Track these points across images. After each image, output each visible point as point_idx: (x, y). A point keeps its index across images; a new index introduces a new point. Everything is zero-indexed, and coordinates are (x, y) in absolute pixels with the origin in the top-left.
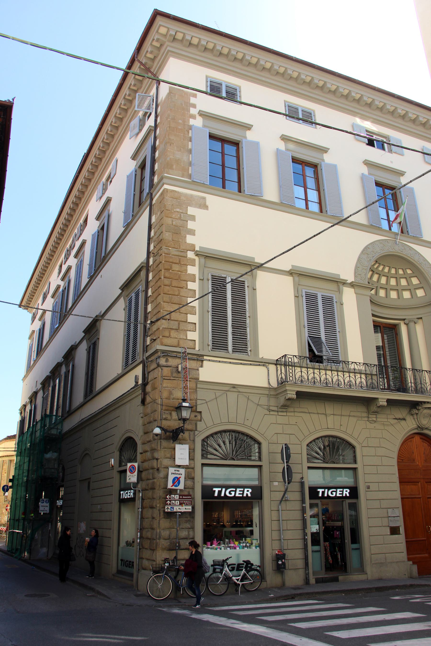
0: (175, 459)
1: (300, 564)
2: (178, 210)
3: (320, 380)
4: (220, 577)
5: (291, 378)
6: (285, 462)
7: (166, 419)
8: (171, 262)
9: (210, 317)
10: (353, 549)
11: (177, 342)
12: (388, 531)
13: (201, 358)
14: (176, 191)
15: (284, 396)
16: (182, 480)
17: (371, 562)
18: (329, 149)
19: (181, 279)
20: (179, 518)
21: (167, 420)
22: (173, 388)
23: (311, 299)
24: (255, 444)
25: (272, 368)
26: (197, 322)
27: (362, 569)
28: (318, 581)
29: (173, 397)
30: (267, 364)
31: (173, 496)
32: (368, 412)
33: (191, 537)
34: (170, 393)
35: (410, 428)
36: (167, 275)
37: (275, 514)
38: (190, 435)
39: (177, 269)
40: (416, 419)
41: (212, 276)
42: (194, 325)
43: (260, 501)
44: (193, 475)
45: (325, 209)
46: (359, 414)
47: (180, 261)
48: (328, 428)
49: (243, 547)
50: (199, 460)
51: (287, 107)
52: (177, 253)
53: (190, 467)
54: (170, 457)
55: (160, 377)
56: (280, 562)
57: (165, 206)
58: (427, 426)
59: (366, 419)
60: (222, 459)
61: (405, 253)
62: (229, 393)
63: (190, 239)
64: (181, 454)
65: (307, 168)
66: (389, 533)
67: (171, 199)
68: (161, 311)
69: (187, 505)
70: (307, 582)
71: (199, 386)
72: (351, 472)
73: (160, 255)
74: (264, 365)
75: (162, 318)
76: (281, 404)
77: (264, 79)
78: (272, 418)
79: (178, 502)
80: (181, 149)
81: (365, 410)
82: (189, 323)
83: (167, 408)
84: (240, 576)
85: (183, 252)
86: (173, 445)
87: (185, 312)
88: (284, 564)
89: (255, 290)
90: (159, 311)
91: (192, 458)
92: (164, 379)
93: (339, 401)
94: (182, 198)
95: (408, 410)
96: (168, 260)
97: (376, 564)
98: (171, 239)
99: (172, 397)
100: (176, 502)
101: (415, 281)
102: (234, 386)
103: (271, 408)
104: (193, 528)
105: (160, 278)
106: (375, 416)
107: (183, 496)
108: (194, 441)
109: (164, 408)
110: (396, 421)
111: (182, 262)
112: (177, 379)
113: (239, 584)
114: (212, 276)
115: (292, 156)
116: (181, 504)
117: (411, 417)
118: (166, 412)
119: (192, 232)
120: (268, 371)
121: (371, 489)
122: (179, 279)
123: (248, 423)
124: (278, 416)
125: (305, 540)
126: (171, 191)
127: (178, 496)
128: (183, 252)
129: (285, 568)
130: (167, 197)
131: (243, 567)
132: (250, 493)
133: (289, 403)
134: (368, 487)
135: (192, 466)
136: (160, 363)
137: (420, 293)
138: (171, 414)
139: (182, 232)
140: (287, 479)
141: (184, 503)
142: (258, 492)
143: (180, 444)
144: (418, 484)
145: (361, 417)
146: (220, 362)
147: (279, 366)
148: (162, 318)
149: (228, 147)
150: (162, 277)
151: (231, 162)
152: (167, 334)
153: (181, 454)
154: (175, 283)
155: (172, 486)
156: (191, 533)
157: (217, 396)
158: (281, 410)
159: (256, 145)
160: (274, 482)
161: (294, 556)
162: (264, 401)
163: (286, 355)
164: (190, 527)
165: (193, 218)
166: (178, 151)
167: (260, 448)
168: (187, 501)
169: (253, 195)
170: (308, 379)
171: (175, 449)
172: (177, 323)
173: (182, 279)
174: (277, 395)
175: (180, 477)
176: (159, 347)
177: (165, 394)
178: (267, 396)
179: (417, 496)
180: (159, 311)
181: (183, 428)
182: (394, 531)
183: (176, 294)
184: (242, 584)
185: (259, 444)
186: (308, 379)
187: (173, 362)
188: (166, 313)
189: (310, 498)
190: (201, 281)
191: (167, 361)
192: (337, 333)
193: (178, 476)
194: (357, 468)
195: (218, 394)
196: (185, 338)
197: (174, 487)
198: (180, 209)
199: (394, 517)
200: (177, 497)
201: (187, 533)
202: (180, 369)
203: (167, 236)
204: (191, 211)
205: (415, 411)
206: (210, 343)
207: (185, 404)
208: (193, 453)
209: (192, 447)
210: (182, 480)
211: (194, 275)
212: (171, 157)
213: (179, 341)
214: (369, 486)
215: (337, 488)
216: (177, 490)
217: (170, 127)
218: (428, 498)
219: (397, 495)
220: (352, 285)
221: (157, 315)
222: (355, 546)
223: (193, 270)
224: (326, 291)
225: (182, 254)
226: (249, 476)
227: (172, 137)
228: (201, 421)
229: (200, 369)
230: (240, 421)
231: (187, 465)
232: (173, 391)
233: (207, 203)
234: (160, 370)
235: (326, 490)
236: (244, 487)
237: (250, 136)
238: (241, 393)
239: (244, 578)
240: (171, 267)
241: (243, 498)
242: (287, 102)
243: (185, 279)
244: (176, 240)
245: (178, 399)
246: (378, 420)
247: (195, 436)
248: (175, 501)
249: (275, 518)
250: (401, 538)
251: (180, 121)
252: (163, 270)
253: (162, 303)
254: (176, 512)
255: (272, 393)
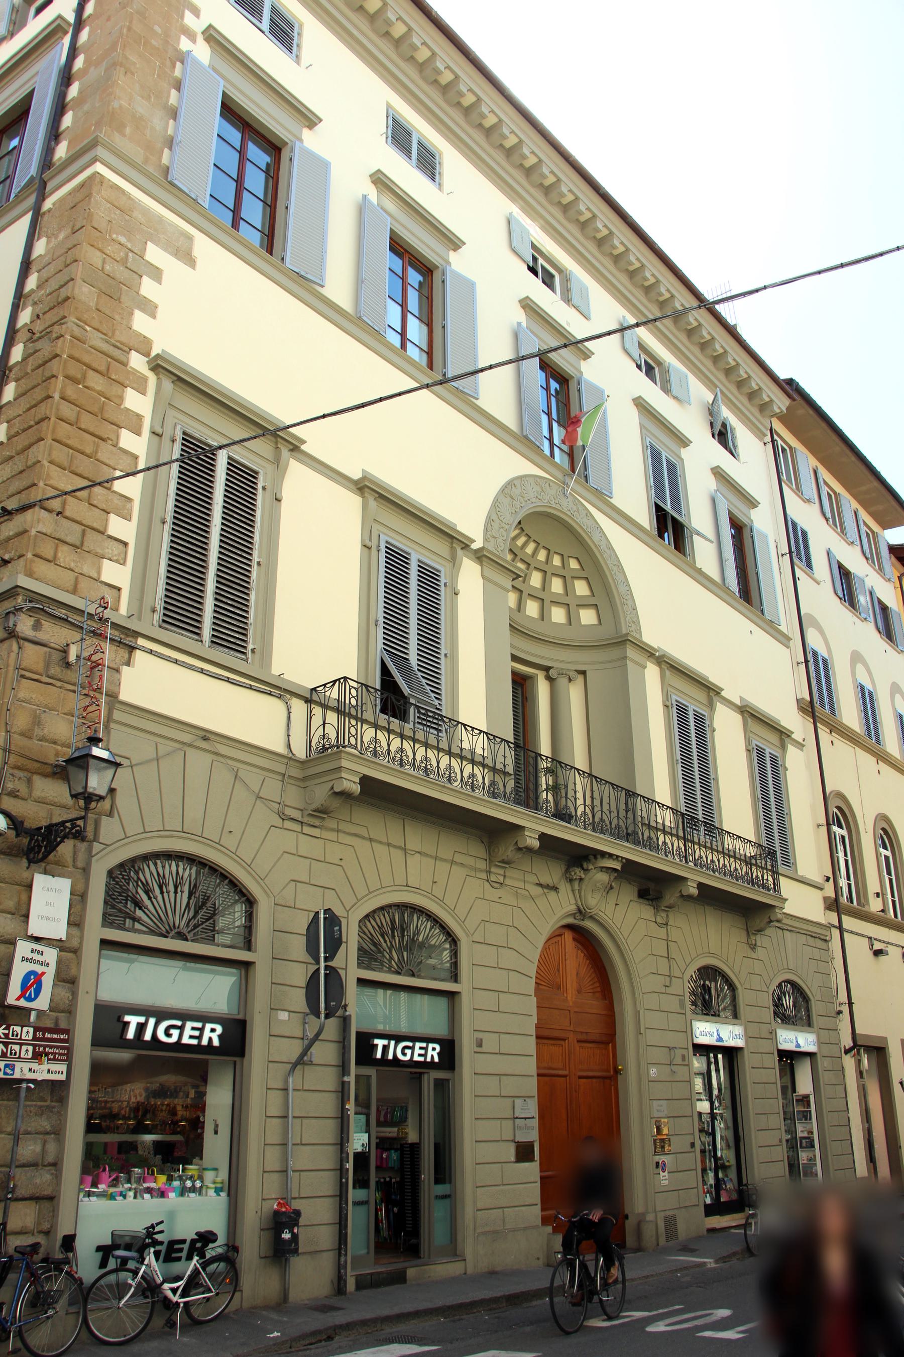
0: (27, 916)
1: (325, 1237)
2: (123, 240)
3: (414, 758)
4: (131, 1286)
5: (353, 741)
6: (322, 959)
7: (13, 794)
8: (85, 364)
9: (167, 538)
10: (437, 1197)
11: (72, 582)
12: (510, 1152)
13: (128, 640)
14: (123, 191)
15: (331, 784)
16: (48, 982)
17: (475, 1229)
18: (465, 244)
19: (106, 416)
20: (27, 1098)
21: (16, 797)
22: (46, 706)
23: (396, 561)
24: (236, 902)
25: (299, 707)
26: (131, 541)
27: (453, 1251)
28: (361, 1285)
29: (41, 733)
30: (288, 696)
31: (18, 1029)
32: (490, 860)
33: (50, 1158)
34: (37, 721)
35: (565, 911)
36: (70, 392)
37: (275, 1098)
38: (75, 853)
39: (98, 388)
40: (577, 892)
41: (184, 433)
42: (121, 546)
43: (237, 1059)
44: (73, 971)
45: (440, 372)
46: (470, 861)
47: (108, 369)
48: (407, 886)
49: (183, 1192)
50: (95, 929)
51: (390, 119)
52: (105, 347)
53: (67, 945)
54: (13, 910)
55: (11, 668)
56: (286, 1236)
57: (90, 217)
58: (594, 911)
59: (484, 876)
60: (152, 932)
61: (579, 522)
62: (190, 752)
63: (140, 322)
64: (48, 904)
65: (417, 268)
66: (513, 1159)
67: (108, 205)
68: (41, 484)
69: (54, 1059)
70: (340, 1288)
71: (117, 715)
72: (442, 1003)
73: (58, 338)
74: (280, 697)
75: (41, 503)
76: (314, 806)
77: (355, 32)
78: (288, 838)
79: (30, 1048)
80: (150, 97)
81: (482, 853)
82: (110, 537)
83: (21, 761)
84: (181, 1279)
85: (118, 348)
86: (26, 874)
87: (104, 506)
88: (295, 1237)
89: (278, 500)
90: (35, 485)
91: (75, 922)
92: (23, 676)
93: (433, 823)
94: (136, 214)
95: (564, 868)
96: (77, 355)
97: (484, 1233)
98: (92, 304)
99: (38, 732)
100: (24, 1048)
101: (581, 588)
102: (206, 735)
103: (289, 812)
104: (58, 1133)
105: (49, 397)
106: (501, 871)
107: (45, 1030)
108: (86, 871)
109: (13, 759)
110: (540, 889)
111: (116, 375)
112: (59, 684)
113: (178, 1304)
114: (184, 433)
115: (392, 231)
116: (37, 1056)
117: (568, 885)
118: (17, 772)
119: (150, 309)
120: (290, 712)
121: (484, 1048)
122: (99, 414)
123: (230, 842)
124: (300, 836)
125: (342, 1171)
126: (111, 187)
127: (31, 1030)
128: (118, 348)
129: (296, 1251)
130: (99, 198)
131: (181, 1250)
132: (219, 1036)
133: (336, 803)
134: (480, 1044)
135: (75, 943)
136: (18, 629)
137: (588, 617)
138: (29, 781)
139: (124, 298)
140: (322, 1005)
141: (47, 1054)
142: (236, 1036)
143: (46, 872)
144: (563, 1043)
145: (475, 870)
146: (176, 662)
147: (317, 711)
148: (41, 503)
149: (261, 144)
150: (57, 396)
151: (255, 181)
152: (47, 550)
153: (48, 904)
154: (87, 421)
155: (18, 999)
156: (52, 1147)
157: (160, 754)
158: (307, 819)
159: (322, 167)
160: (280, 1012)
161: (317, 1216)
162: (273, 789)
163: (345, 678)
164: (48, 1128)
165: (157, 274)
166: (143, 97)
167: (250, 916)
168: (57, 1047)
169: (301, 276)
170: (389, 750)
171: (30, 887)
172: (79, 528)
173: (109, 418)
174: (305, 779)
175: (43, 973)
176: (24, 581)
177: (21, 721)
178: (280, 778)
179: (560, 1072)
180: (35, 485)
181: (80, 823)
182: (524, 1153)
183: (88, 451)
184: (185, 1303)
185: (250, 902)
186: (389, 750)
187: (54, 633)
188: (51, 492)
189: (358, 1063)
190: (156, 438)
191: (37, 626)
192: (442, 657)
193: (39, 969)
194: (459, 993)
195: (162, 750)
196: (95, 576)
197: (23, 1003)
198: (129, 240)
199: (526, 1118)
200: (27, 1033)
201: (38, 1148)
202: (72, 658)
203: (84, 293)
204: (154, 254)
205: (578, 872)
206: (159, 605)
207: (96, 751)
208: (79, 907)
209: (80, 887)
210: (48, 982)
211: (139, 417)
212: (124, 104)
213: (77, 578)
214: (481, 1040)
215: (414, 1039)
216: (28, 1011)
217: (129, 29)
218: (580, 1077)
219: (530, 1066)
220: (480, 556)
221: (23, 495)
222: (441, 1189)
223: (138, 402)
224: (428, 554)
225: (116, 353)
226: (213, 991)
227: (133, 58)
228: (110, 814)
229: (125, 669)
230: (212, 832)
231: (61, 940)
232: (43, 715)
233: (196, 253)
234: (15, 647)
235: (393, 1043)
236: (204, 1018)
237: (310, 140)
238: (221, 759)
239: (193, 1284)
240: (84, 377)
241: (198, 1049)
242: (392, 108)
243: (115, 420)
244: (107, 312)
245: (55, 743)
246: (508, 882)
247: (90, 856)
248: (21, 1045)
249: (274, 1111)
250: (532, 1170)
251: (158, 29)
252: (61, 378)
253: (46, 463)
254: (20, 1081)
255: (295, 772)
